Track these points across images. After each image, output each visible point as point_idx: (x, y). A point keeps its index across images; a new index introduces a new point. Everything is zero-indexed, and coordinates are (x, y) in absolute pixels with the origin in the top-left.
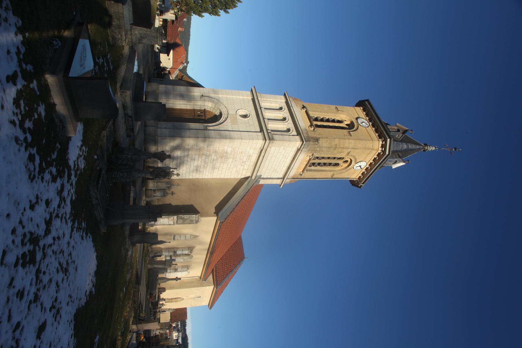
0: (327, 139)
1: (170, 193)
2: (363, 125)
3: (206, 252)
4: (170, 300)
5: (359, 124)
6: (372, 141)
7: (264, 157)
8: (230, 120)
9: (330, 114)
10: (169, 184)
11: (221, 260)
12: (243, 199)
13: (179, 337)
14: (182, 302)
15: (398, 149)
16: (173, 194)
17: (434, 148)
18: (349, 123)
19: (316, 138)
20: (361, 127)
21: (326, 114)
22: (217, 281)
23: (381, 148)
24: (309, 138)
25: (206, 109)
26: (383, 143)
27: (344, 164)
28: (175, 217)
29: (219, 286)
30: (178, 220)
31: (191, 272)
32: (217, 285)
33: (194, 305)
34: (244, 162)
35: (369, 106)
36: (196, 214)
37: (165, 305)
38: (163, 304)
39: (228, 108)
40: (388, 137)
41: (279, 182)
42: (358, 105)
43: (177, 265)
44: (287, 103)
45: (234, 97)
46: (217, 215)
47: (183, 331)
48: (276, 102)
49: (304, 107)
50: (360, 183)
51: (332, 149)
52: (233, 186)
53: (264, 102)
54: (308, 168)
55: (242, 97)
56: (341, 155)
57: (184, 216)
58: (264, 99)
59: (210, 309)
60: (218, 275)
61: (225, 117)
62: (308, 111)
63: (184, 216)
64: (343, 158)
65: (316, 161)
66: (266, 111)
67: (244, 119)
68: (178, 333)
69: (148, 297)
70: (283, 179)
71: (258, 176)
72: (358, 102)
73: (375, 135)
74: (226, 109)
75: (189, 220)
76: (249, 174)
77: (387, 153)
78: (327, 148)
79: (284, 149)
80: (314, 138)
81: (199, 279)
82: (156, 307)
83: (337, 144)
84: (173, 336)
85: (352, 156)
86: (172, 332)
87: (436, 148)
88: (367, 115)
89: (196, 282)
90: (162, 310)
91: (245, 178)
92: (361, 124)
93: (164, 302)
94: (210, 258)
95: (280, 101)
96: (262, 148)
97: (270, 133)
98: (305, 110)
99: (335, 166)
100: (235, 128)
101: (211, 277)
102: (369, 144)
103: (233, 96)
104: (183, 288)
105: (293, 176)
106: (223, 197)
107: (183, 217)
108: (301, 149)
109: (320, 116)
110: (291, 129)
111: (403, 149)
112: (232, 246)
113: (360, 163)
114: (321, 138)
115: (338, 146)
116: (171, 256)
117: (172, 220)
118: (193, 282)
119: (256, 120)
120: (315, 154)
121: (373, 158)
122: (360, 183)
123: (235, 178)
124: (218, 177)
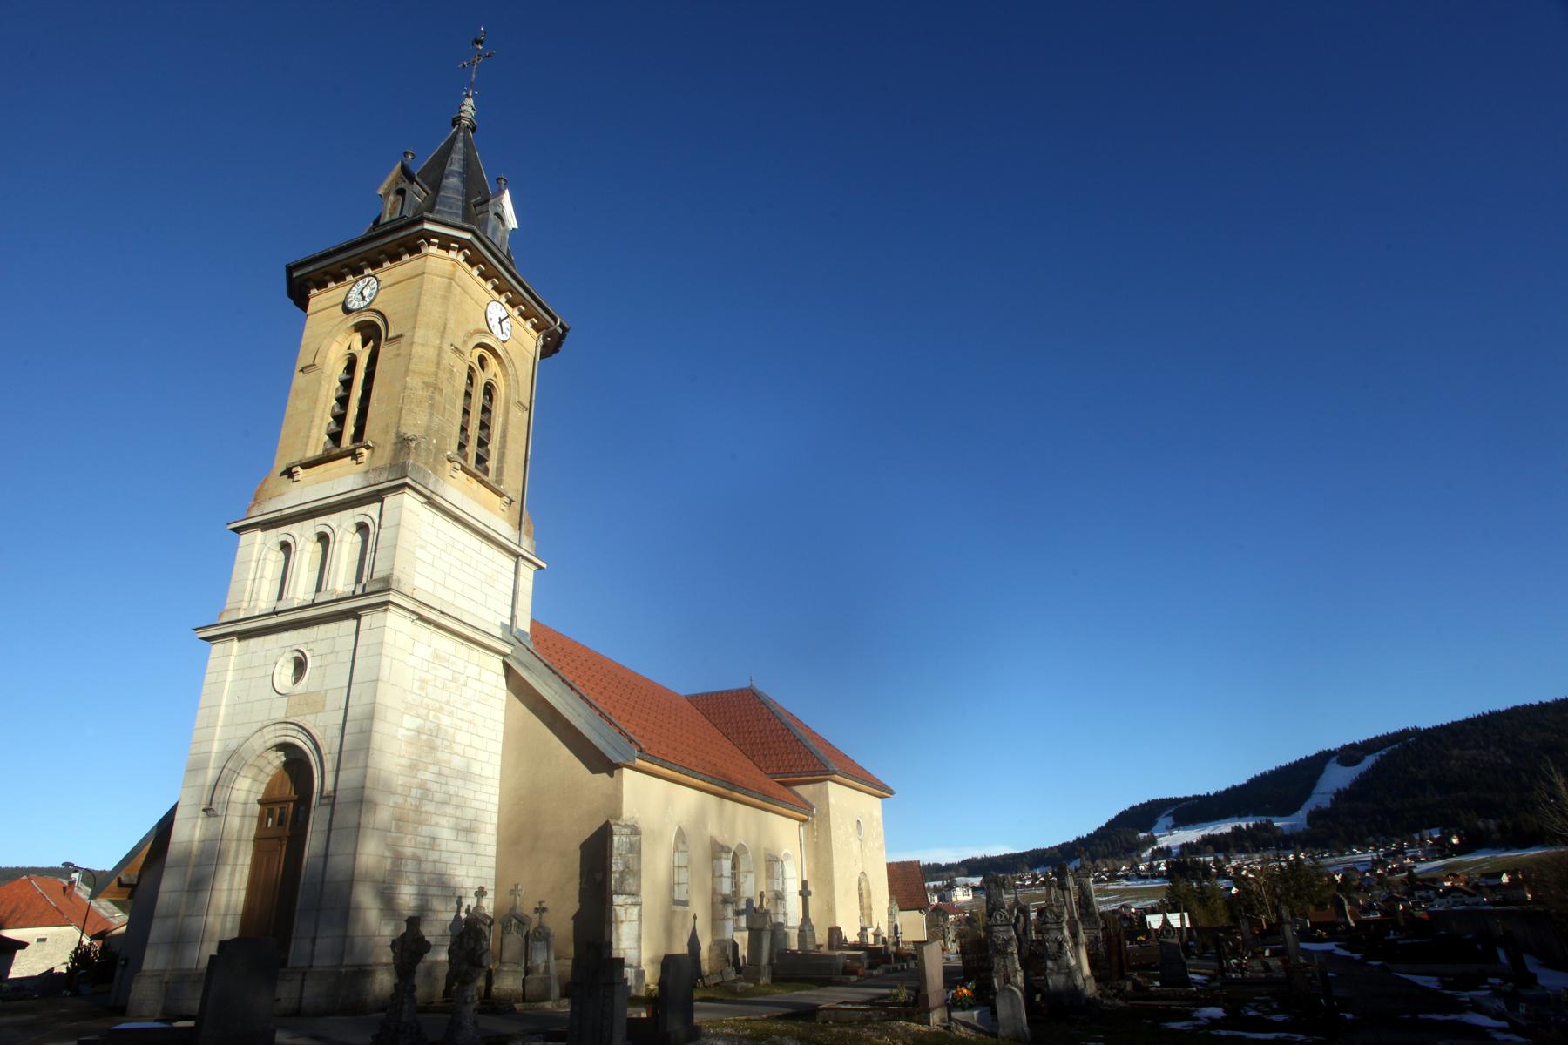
0: (404, 412)
2: (371, 295)
3: (728, 803)
4: (866, 911)
5: (364, 307)
7: (442, 613)
8: (308, 717)
9: (323, 392)
10: (510, 921)
12: (572, 684)
13: (967, 885)
15: (460, 203)
16: (544, 910)
17: (470, 102)
18: (357, 338)
19: (396, 444)
22: (813, 773)
25: (260, 797)
26: (434, 244)
28: (617, 900)
30: (628, 890)
31: (786, 851)
33: (881, 841)
34: (456, 675)
35: (311, 268)
39: (262, 721)
41: (527, 572)
42: (302, 301)
44: (267, 525)
46: (619, 766)
47: (952, 873)
49: (289, 473)
51: (437, 397)
54: (491, 478)
58: (246, 598)
59: (891, 792)
63: (615, 872)
65: (473, 452)
66: (290, 596)
68: (957, 886)
69: (854, 978)
73: (409, 264)
74: (265, 730)
75: (630, 855)
76: (496, 664)
77: (468, 236)
78: (431, 415)
79: (422, 547)
80: (395, 450)
81: (806, 826)
83: (424, 383)
87: (468, 96)
88: (339, 278)
89: (816, 834)
90: (892, 935)
91: (507, 676)
92: (368, 300)
93: (870, 931)
94: (747, 791)
98: (299, 469)
99: (494, 397)
102: (434, 284)
103: (224, 703)
105: (512, 525)
107: (617, 876)
113: (491, 319)
115: (431, 380)
116: (738, 913)
117: (626, 910)
118: (816, 843)
120: (449, 453)
122: (552, 329)
123: (504, 708)
124: (497, 760)
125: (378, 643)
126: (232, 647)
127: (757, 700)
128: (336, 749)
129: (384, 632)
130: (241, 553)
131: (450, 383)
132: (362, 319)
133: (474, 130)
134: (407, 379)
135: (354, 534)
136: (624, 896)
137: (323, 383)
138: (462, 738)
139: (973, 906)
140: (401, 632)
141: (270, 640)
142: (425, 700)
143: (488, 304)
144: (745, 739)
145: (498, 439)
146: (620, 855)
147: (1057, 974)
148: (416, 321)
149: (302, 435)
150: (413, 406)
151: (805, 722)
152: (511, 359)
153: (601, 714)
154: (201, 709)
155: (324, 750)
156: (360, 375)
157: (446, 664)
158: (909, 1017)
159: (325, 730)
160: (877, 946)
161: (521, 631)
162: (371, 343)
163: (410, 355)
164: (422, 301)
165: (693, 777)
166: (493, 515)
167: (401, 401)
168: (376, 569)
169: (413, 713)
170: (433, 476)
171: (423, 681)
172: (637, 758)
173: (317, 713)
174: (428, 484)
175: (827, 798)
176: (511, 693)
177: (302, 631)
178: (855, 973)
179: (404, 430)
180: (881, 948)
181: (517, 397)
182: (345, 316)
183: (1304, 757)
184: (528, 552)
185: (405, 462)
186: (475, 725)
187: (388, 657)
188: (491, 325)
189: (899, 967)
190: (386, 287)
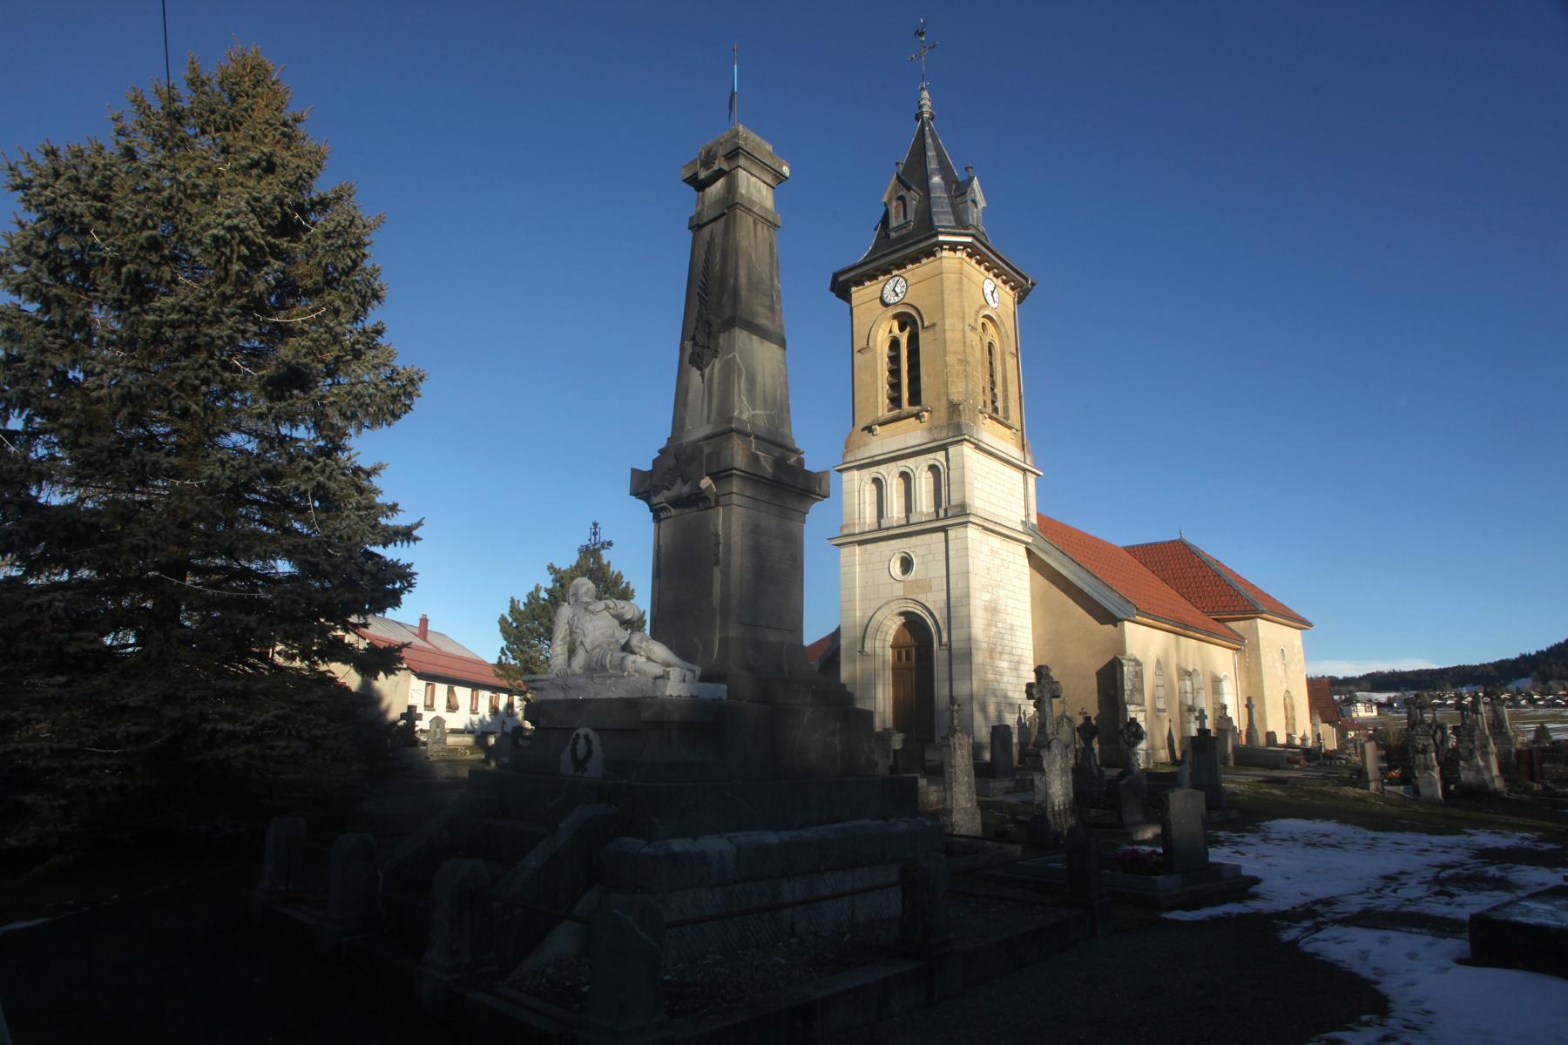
0: (949, 384)
2: (902, 292)
3: (1182, 638)
4: (1290, 721)
8: (920, 596)
10: (1062, 720)
13: (1370, 701)
14: (1293, 694)
15: (947, 201)
17: (925, 94)
18: (896, 325)
19: (948, 408)
20: (907, 297)
21: (880, 377)
22: (1244, 612)
23: (958, 252)
25: (891, 643)
26: (945, 249)
30: (1136, 702)
31: (1225, 673)
35: (852, 274)
36: (1121, 665)
40: (934, 240)
41: (1031, 479)
42: (845, 295)
43: (411, 708)
44: (860, 467)
46: (1122, 620)
47: (1352, 688)
49: (869, 429)
53: (864, 518)
54: (1001, 414)
55: (857, 567)
58: (857, 516)
59: (1310, 625)
61: (913, 605)
68: (1357, 702)
69: (1297, 766)
73: (927, 265)
74: (892, 603)
76: (1021, 549)
77: (969, 240)
78: (967, 383)
83: (959, 360)
84: (1369, 718)
85: (976, 320)
86: (1353, 720)
87: (923, 89)
89: (1248, 660)
90: (1316, 740)
91: (1029, 557)
92: (901, 296)
94: (1196, 630)
96: (980, 528)
97: (946, 510)
98: (877, 427)
99: (993, 352)
102: (950, 280)
104: (1263, 693)
106: (1078, 607)
107: (1129, 692)
108: (976, 442)
111: (943, 185)
112: (1153, 572)
118: (1248, 667)
119: (914, 538)
120: (980, 407)
121: (977, 266)
122: (1025, 287)
124: (1029, 615)
132: (899, 310)
133: (932, 119)
138: (1011, 603)
139: (1378, 723)
144: (1217, 603)
147: (1469, 770)
148: (943, 313)
155: (937, 617)
157: (997, 556)
158: (1354, 785)
161: (1033, 524)
162: (908, 329)
163: (945, 340)
171: (988, 569)
176: (1035, 573)
177: (904, 540)
179: (951, 397)
182: (885, 309)
183: (1527, 654)
188: (987, 298)
189: (1328, 763)
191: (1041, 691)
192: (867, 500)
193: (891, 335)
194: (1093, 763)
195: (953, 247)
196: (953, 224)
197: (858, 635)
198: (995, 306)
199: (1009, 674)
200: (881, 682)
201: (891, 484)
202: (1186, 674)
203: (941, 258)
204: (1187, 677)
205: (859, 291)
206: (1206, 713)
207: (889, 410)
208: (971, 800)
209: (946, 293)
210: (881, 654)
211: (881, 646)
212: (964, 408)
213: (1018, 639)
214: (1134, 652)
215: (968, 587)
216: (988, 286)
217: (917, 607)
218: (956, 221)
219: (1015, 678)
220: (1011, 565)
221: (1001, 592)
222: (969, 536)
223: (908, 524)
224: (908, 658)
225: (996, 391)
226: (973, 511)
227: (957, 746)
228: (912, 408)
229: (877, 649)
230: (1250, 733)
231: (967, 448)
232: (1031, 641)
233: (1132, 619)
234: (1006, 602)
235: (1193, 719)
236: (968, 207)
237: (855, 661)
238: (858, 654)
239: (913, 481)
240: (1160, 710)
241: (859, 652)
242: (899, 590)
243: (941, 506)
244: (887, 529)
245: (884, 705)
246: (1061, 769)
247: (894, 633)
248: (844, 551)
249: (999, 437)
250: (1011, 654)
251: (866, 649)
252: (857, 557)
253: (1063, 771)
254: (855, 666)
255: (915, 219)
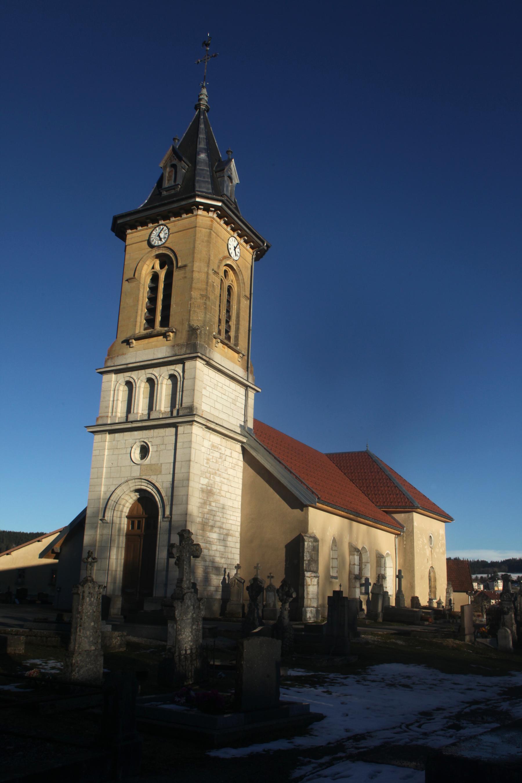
0: (191, 312)
1: (270, 581)
2: (165, 238)
3: (355, 524)
4: (433, 590)
5: (161, 245)
6: (197, 228)
7: (217, 424)
8: (152, 477)
9: (141, 295)
11: (354, 482)
12: (290, 469)
14: (436, 570)
15: (208, 173)
16: (272, 577)
17: (204, 91)
18: (157, 264)
19: (189, 331)
20: (167, 242)
21: (140, 302)
23: (210, 213)
24: (189, 344)
25: (127, 514)
26: (201, 209)
27: (230, 277)
28: (307, 574)
29: (414, 504)
30: (312, 569)
31: (388, 552)
32: (413, 507)
33: (444, 548)
34: (221, 455)
35: (128, 219)
36: (303, 541)
37: (440, 599)
38: (439, 603)
39: (127, 477)
40: (193, 200)
41: (251, 394)
42: (123, 237)
44: (117, 372)
45: (105, 465)
46: (307, 506)
47: (496, 569)
48: (116, 391)
49: (127, 342)
50: (261, 248)
51: (208, 303)
52: (257, 475)
53: (116, 412)
55: (106, 451)
56: (216, 286)
57: (305, 560)
59: (451, 519)
60: (396, 504)
61: (146, 485)
62: (136, 337)
63: (305, 560)
64: (222, 280)
65: (223, 329)
66: (135, 411)
67: (150, 453)
69: (426, 623)
70: (248, 387)
71: (241, 431)
72: (114, 234)
73: (185, 220)
74: (130, 482)
75: (313, 552)
76: (238, 447)
77: (220, 204)
78: (206, 314)
79: (205, 388)
80: (188, 335)
81: (399, 538)
82: (442, 613)
83: (201, 295)
85: (219, 267)
87: (203, 87)
88: (144, 224)
89: (405, 543)
92: (163, 241)
93: (435, 601)
95: (113, 382)
97: (178, 410)
98: (134, 341)
99: (231, 293)
100: (168, 468)
101: (398, 517)
102: (202, 233)
103: (105, 466)
105: (243, 369)
106: (276, 494)
107: (307, 562)
108: (207, 359)
109: (143, 315)
110: (172, 372)
111: (208, 162)
112: (345, 474)
113: (230, 248)
114: (189, 322)
115: (204, 293)
116: (361, 585)
117: (311, 579)
118: (405, 548)
119: (152, 431)
120: (214, 333)
122: (261, 248)
123: (242, 471)
124: (239, 498)
125: (189, 441)
126: (106, 437)
127: (371, 460)
128: (170, 494)
129: (192, 436)
130: (104, 385)
131: (213, 292)
132: (161, 252)
133: (207, 111)
134: (192, 293)
135: (168, 380)
136: (310, 573)
137: (140, 289)
138: (225, 488)
140: (198, 435)
141: (127, 435)
142: (209, 469)
143: (228, 240)
145: (235, 319)
146: (308, 552)
148: (193, 257)
149: (132, 320)
150: (196, 309)
151: (400, 474)
152: (240, 270)
153: (296, 477)
154: (93, 468)
155: (163, 494)
156: (161, 286)
158: (455, 638)
159: (163, 484)
160: (440, 609)
161: (249, 428)
162: (166, 267)
163: (192, 278)
164: (196, 244)
165: (342, 511)
166: (235, 365)
167: (189, 306)
168: (184, 402)
169: (204, 476)
170: (208, 349)
171: (208, 459)
172: (318, 503)
173: (157, 475)
174: (206, 353)
175: (413, 522)
177: (145, 432)
178: (427, 620)
179: (192, 323)
180: (441, 610)
181: (244, 293)
182: (151, 249)
184: (253, 384)
185: (195, 343)
186: (230, 480)
187: (194, 448)
188: (230, 252)
190: (173, 233)
191: (180, 551)
192: (120, 398)
193: (153, 270)
194: (256, 615)
195: (207, 208)
196: (210, 191)
197: (101, 506)
198: (236, 258)
199: (218, 544)
200: (116, 545)
201: (139, 387)
202: (354, 550)
203: (196, 215)
204: (356, 553)
205: (132, 233)
206: (370, 581)
207: (145, 329)
208: (95, 644)
209: (198, 242)
210: (118, 522)
211: (119, 516)
212: (201, 332)
213: (228, 517)
214: (315, 531)
215: (189, 472)
216: (233, 243)
217: (149, 486)
218: (212, 189)
219: (222, 547)
220: (228, 459)
221: (218, 479)
222: (193, 432)
223: (149, 419)
224: (139, 527)
225: (230, 323)
226: (200, 413)
227: (86, 594)
228: (162, 328)
229: (114, 518)
230: (399, 597)
231: (199, 364)
232: (239, 519)
233: (314, 505)
234: (221, 487)
235: (358, 585)
236: (224, 181)
237: (96, 527)
238: (100, 522)
239: (156, 386)
240: (333, 577)
241: (101, 520)
242: (136, 472)
243: (175, 407)
244: (132, 422)
245: (117, 566)
246: (193, 618)
247: (130, 506)
248: (97, 437)
249: (228, 359)
250: (220, 528)
251: (106, 518)
252: (107, 443)
253: (194, 620)
254: (96, 531)
255: (182, 184)
